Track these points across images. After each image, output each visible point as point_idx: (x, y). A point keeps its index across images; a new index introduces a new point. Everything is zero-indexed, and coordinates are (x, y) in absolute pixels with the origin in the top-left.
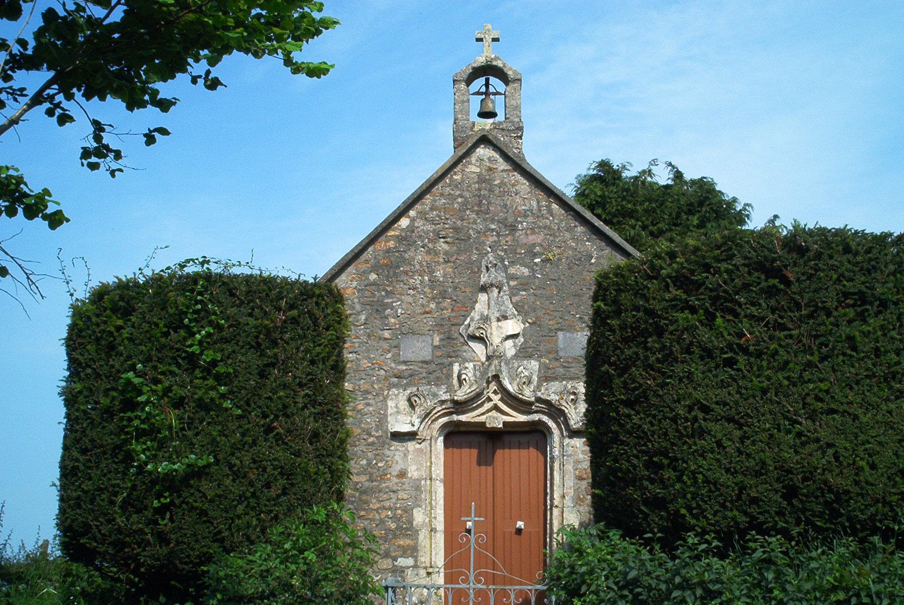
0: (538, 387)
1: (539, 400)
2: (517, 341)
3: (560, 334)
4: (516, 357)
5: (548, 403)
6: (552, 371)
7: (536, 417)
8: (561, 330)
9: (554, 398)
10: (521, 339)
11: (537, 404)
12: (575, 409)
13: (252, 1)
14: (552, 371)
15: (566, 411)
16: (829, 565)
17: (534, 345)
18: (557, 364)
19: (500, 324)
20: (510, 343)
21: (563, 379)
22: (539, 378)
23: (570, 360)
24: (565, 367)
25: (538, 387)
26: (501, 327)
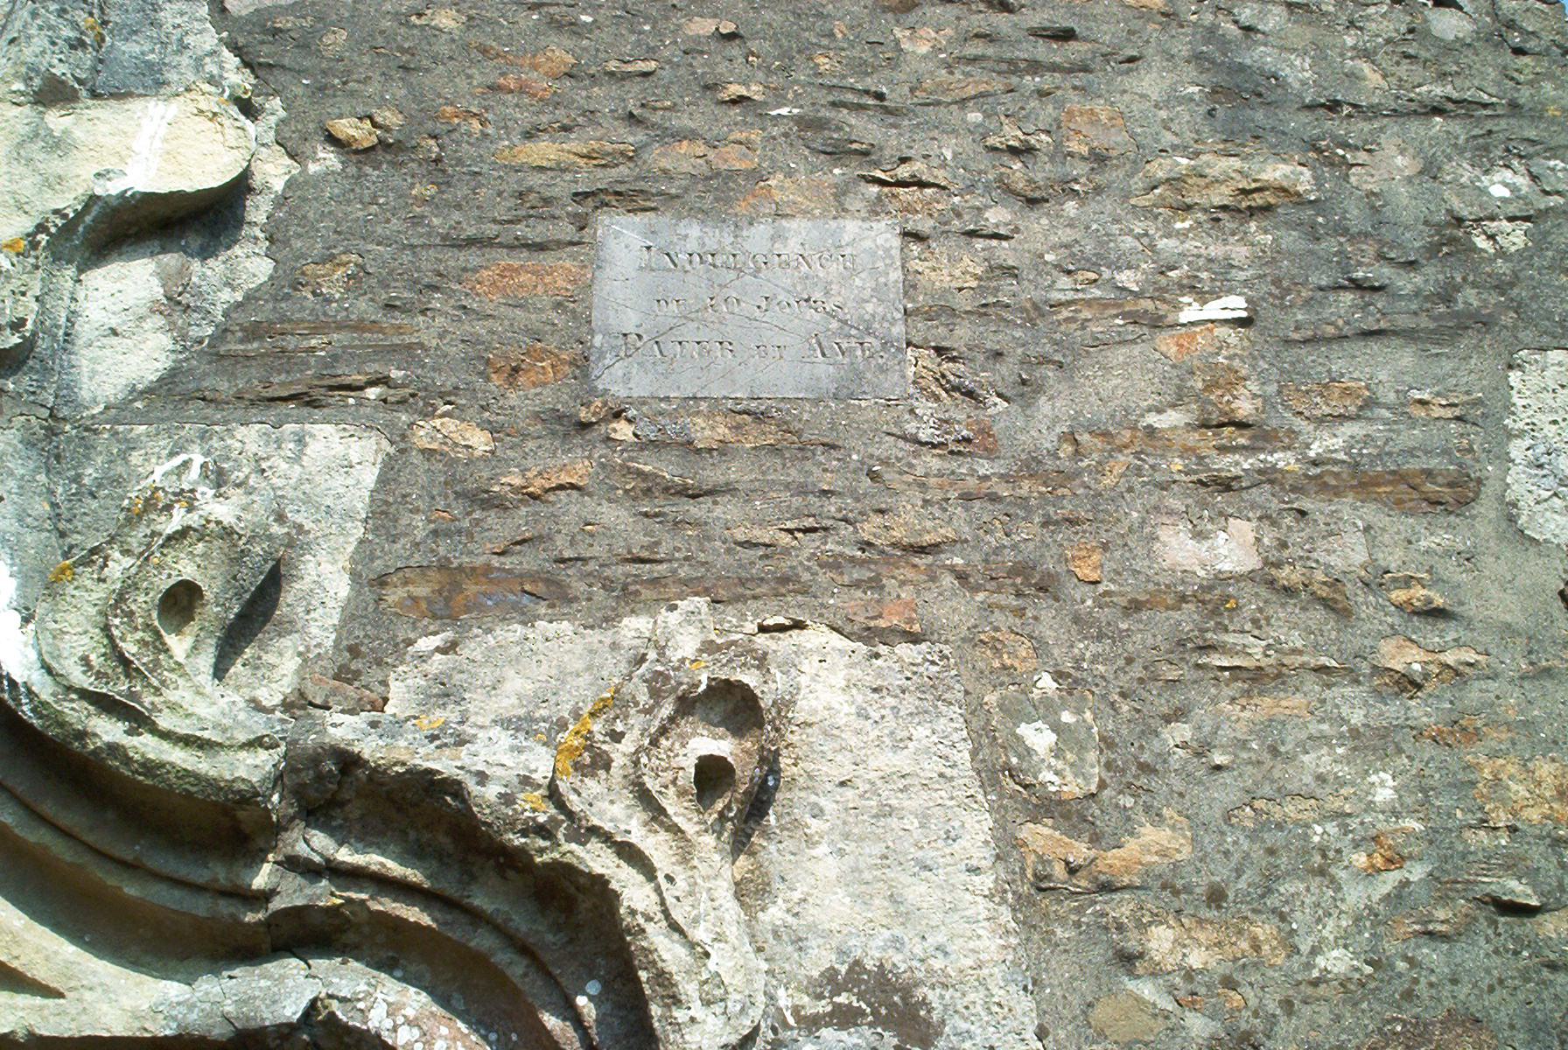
0: (356, 665)
1: (336, 788)
2: (207, 273)
3: (623, 238)
4: (170, 395)
5: (421, 810)
6: (520, 521)
7: (284, 990)
8: (629, 199)
9: (497, 765)
10: (251, 263)
11: (318, 844)
12: (751, 892)
13: (409, 1048)
14: (520, 521)
15: (634, 893)
16: (682, 71)
17: (363, 307)
18: (578, 466)
19: (56, 120)
20: (132, 281)
21: (627, 597)
22: (372, 581)
23: (705, 432)
24: (650, 486)
25: (356, 665)
26: (58, 145)
